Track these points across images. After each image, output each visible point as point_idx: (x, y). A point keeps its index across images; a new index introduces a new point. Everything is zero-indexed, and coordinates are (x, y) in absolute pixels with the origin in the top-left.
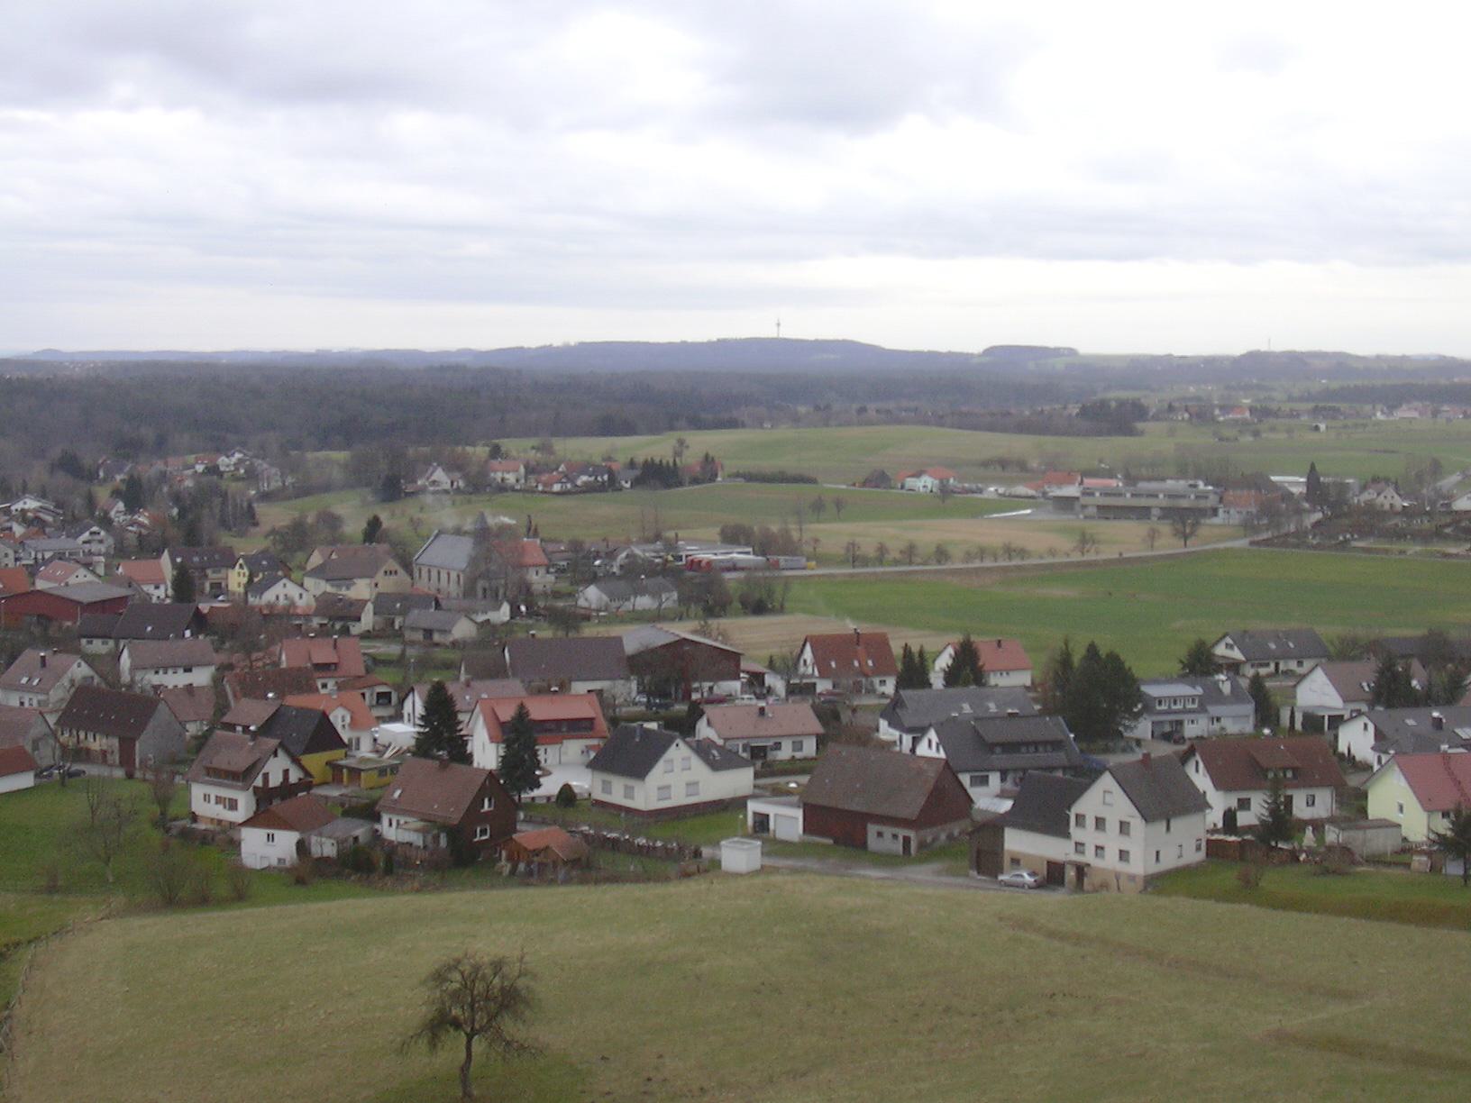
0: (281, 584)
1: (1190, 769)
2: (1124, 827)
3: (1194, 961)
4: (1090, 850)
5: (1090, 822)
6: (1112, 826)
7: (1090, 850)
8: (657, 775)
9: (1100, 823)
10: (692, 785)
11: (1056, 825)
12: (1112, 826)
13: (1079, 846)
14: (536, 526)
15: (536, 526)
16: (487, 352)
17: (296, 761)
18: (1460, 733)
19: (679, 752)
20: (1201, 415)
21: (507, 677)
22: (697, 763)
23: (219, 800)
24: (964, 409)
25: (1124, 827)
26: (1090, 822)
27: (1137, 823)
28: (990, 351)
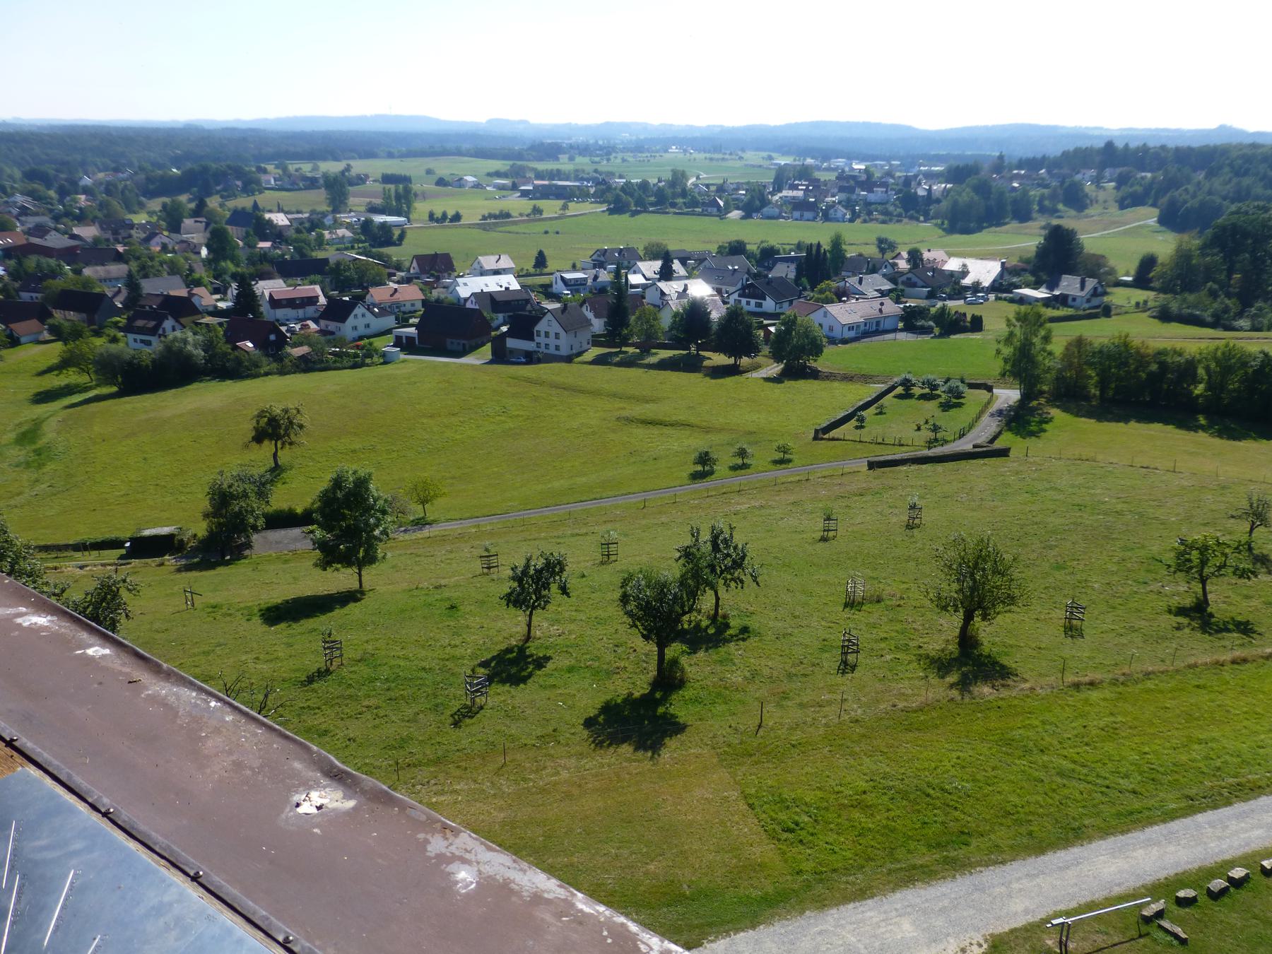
0: (158, 236)
1: (584, 309)
2: (557, 336)
3: (1137, 684)
4: (543, 346)
5: (543, 334)
6: (552, 335)
7: (543, 346)
8: (351, 321)
9: (547, 334)
10: (368, 326)
11: (529, 336)
12: (552, 335)
13: (538, 345)
14: (963, 404)
15: (963, 404)
16: (1043, 126)
17: (177, 321)
18: (883, 385)
19: (359, 310)
20: (584, 150)
21: (407, 337)
22: (368, 314)
23: (142, 341)
24: (1169, 296)
25: (557, 336)
26: (543, 334)
27: (562, 333)
28: (490, 121)
